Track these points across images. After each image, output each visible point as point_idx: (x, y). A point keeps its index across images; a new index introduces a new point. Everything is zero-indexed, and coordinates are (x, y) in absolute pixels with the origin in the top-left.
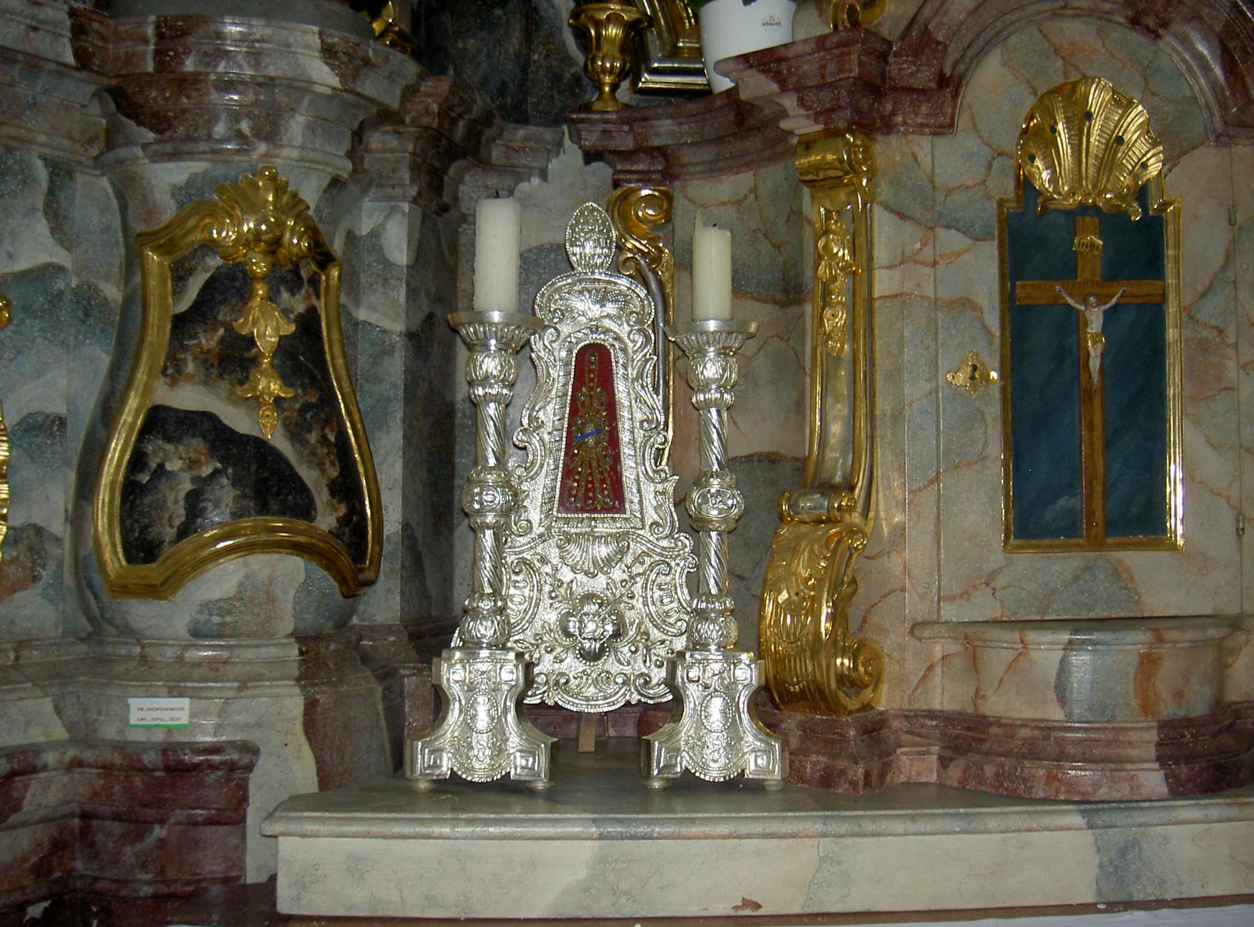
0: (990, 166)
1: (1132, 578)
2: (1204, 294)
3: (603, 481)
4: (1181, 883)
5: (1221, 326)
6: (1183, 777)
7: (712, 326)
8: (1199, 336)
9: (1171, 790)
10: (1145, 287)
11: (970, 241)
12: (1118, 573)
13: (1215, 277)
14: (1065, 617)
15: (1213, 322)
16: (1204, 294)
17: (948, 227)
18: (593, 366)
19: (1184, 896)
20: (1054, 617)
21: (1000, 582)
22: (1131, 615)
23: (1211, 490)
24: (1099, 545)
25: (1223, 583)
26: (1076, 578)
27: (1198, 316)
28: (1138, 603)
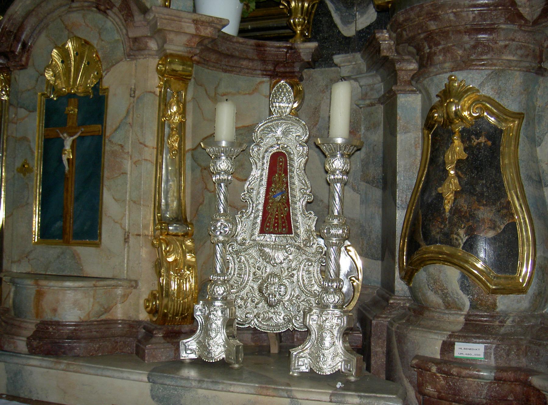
0: (37, 81)
1: (80, 258)
2: (116, 130)
3: (270, 218)
4: (38, 394)
5: (123, 144)
6: (35, 346)
7: (339, 141)
8: (113, 149)
9: (29, 351)
10: (96, 128)
11: (28, 113)
12: (75, 256)
13: (122, 121)
14: (54, 274)
15: (119, 143)
16: (116, 130)
17: (21, 107)
18: (279, 163)
19: (39, 399)
20: (50, 273)
21: (31, 257)
22: (79, 275)
23: (114, 220)
24: (67, 243)
25: (117, 264)
26: (59, 257)
27: (113, 140)
28: (82, 270)
